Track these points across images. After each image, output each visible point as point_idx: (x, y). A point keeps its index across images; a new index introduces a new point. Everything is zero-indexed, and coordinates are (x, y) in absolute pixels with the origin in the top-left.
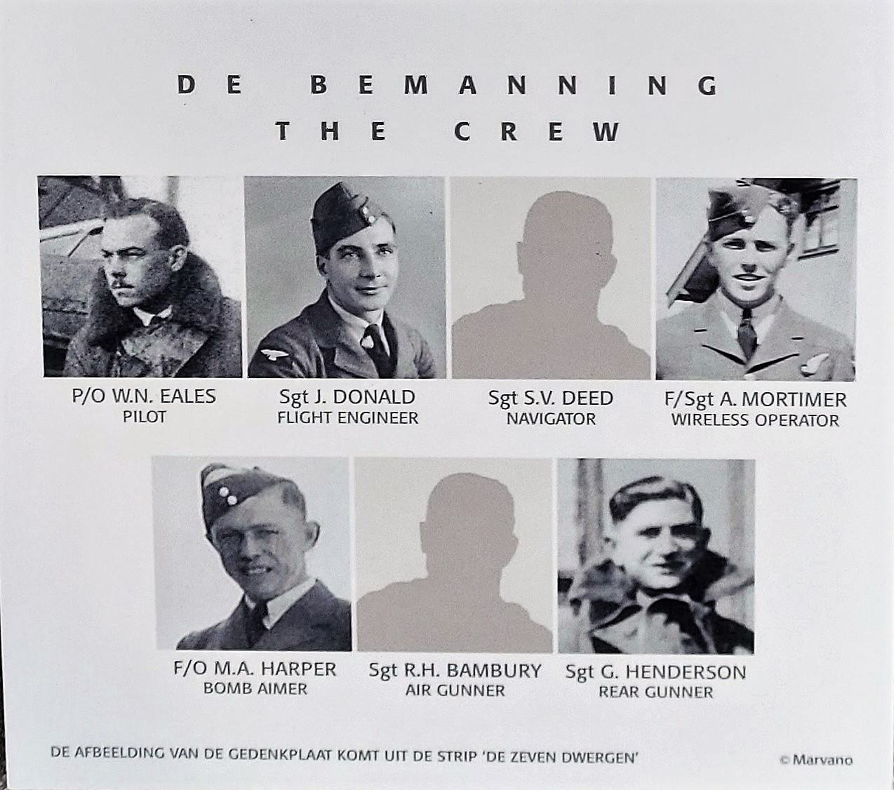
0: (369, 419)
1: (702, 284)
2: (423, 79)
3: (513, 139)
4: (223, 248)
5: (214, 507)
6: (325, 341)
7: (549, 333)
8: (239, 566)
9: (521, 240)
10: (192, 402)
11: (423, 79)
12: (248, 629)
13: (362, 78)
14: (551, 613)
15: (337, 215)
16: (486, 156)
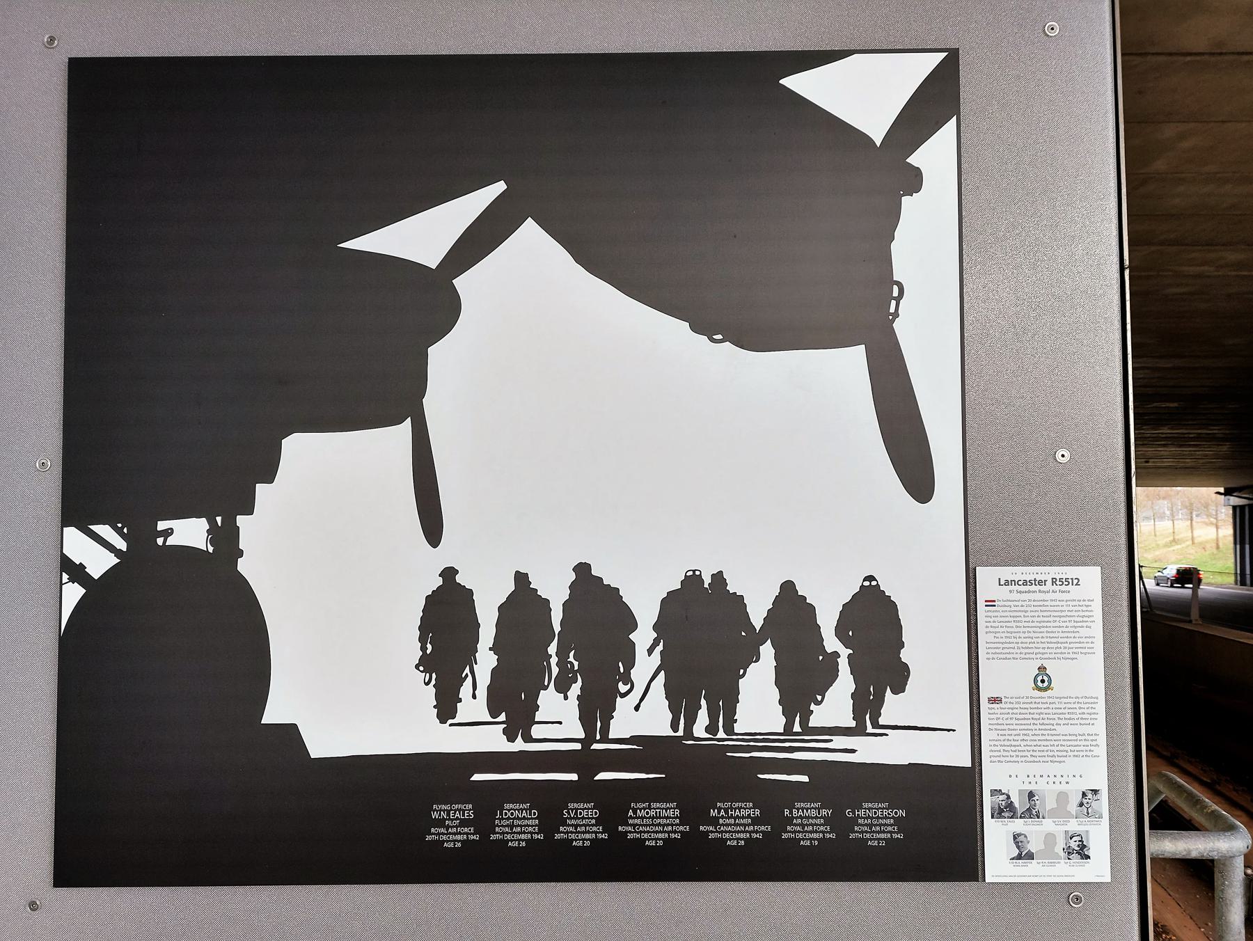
1: (1081, 805)
4: (1015, 800)
5: (1015, 838)
6: (1030, 813)
7: (1060, 812)
8: (1018, 847)
12: (1019, 857)
14: (1062, 854)
15: (1031, 795)
16: (1051, 786)
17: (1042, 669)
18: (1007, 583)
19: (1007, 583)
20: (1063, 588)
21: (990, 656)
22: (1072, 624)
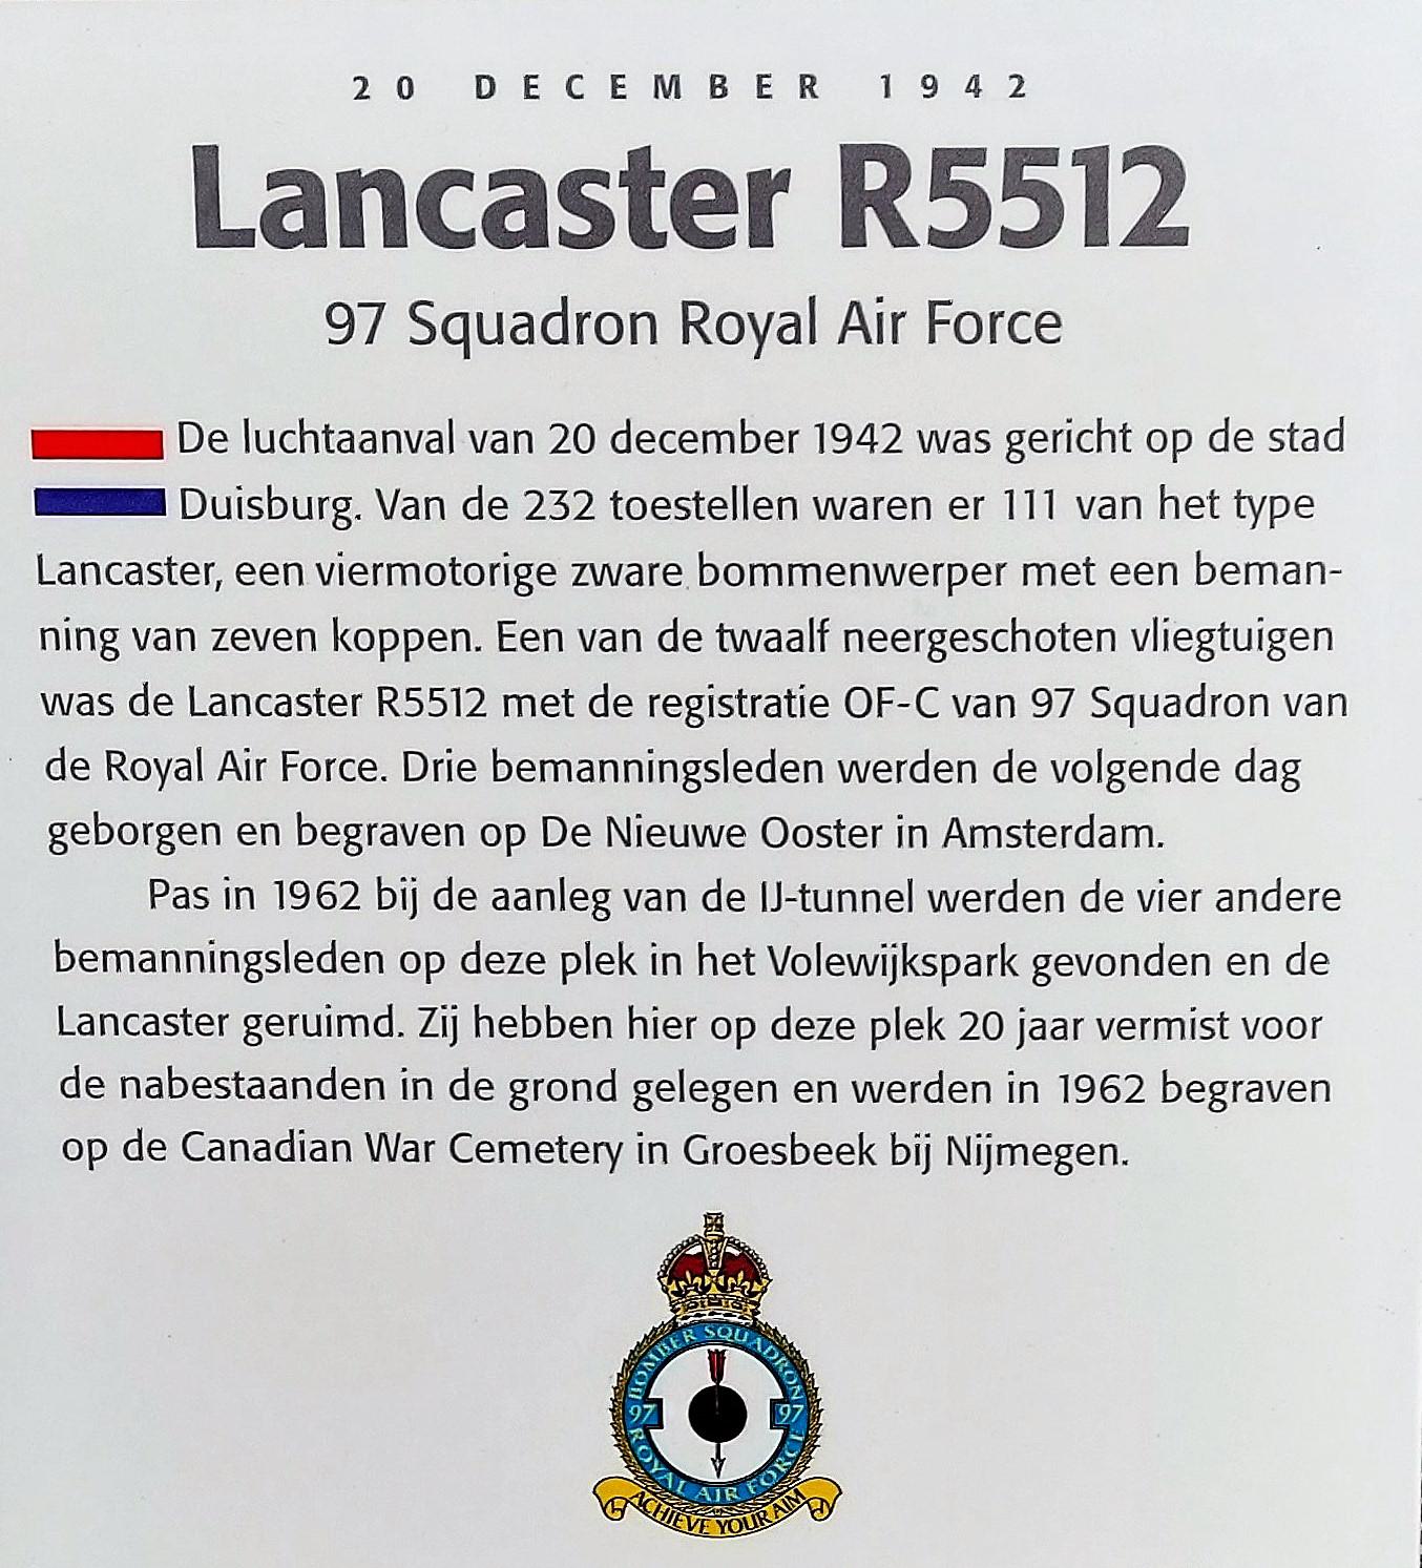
0: (706, 1153)
2: (675, 78)
3: (814, 95)
9: (625, 168)
10: (437, 1035)
11: (675, 78)
13: (760, 77)
17: (714, 1274)
18: (305, 211)
19: (305, 211)
20: (988, 275)
21: (114, 1119)
22: (1079, 734)
